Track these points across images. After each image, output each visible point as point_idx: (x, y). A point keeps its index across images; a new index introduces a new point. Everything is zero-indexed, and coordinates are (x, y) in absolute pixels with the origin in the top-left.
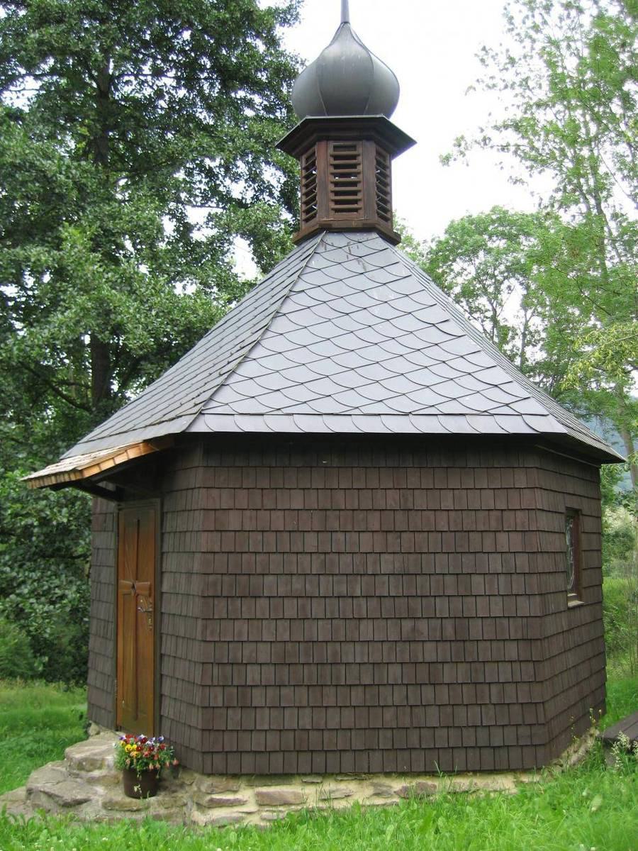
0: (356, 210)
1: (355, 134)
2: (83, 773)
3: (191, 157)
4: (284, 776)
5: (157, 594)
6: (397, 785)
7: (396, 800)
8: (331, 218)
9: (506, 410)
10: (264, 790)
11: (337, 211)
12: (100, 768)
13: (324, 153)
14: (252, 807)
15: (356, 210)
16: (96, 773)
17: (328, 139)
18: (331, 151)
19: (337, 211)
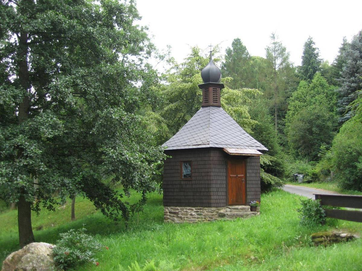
19: (214, 102)
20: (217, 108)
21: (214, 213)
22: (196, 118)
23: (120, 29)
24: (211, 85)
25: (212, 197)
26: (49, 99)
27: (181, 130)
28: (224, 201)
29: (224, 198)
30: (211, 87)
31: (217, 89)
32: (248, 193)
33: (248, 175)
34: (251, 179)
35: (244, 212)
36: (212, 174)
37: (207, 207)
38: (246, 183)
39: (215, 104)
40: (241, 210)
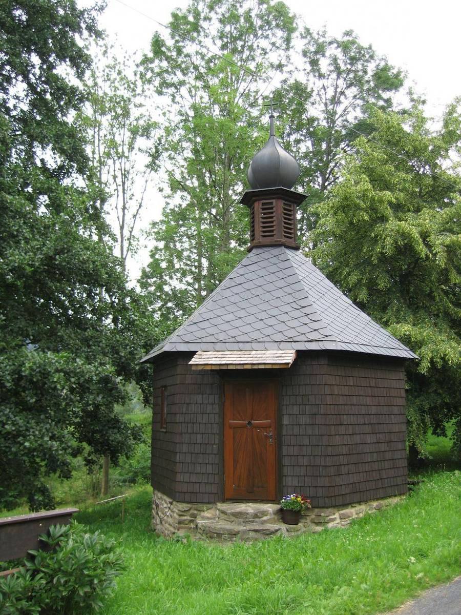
0: (273, 236)
1: (292, 200)
2: (257, 520)
3: (97, 184)
4: (345, 505)
5: (279, 426)
6: (375, 504)
7: (374, 511)
8: (262, 240)
9: (268, 339)
10: (342, 512)
11: (285, 236)
12: (266, 515)
13: (258, 206)
14: (338, 521)
15: (273, 236)
16: (265, 518)
17: (283, 199)
18: (261, 206)
19: (285, 236)
20: (270, 248)
21: (185, 518)
22: (241, 271)
23: (170, 79)
24: (257, 196)
25: (180, 477)
26: (57, 228)
27: (337, 292)
28: (214, 489)
29: (211, 480)
30: (256, 201)
31: (290, 206)
32: (287, 471)
33: (286, 420)
34: (296, 431)
35: (239, 524)
36: (179, 418)
37: (390, 497)
38: (279, 444)
39: (267, 240)
40: (233, 518)
